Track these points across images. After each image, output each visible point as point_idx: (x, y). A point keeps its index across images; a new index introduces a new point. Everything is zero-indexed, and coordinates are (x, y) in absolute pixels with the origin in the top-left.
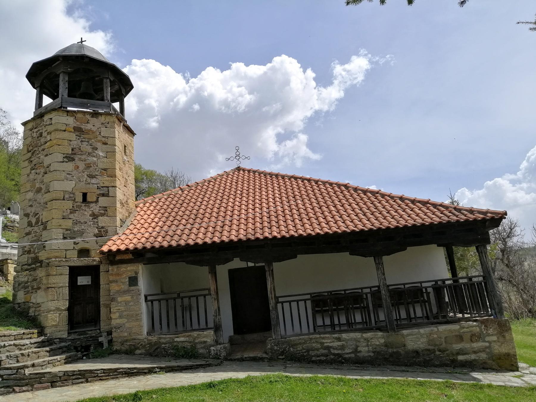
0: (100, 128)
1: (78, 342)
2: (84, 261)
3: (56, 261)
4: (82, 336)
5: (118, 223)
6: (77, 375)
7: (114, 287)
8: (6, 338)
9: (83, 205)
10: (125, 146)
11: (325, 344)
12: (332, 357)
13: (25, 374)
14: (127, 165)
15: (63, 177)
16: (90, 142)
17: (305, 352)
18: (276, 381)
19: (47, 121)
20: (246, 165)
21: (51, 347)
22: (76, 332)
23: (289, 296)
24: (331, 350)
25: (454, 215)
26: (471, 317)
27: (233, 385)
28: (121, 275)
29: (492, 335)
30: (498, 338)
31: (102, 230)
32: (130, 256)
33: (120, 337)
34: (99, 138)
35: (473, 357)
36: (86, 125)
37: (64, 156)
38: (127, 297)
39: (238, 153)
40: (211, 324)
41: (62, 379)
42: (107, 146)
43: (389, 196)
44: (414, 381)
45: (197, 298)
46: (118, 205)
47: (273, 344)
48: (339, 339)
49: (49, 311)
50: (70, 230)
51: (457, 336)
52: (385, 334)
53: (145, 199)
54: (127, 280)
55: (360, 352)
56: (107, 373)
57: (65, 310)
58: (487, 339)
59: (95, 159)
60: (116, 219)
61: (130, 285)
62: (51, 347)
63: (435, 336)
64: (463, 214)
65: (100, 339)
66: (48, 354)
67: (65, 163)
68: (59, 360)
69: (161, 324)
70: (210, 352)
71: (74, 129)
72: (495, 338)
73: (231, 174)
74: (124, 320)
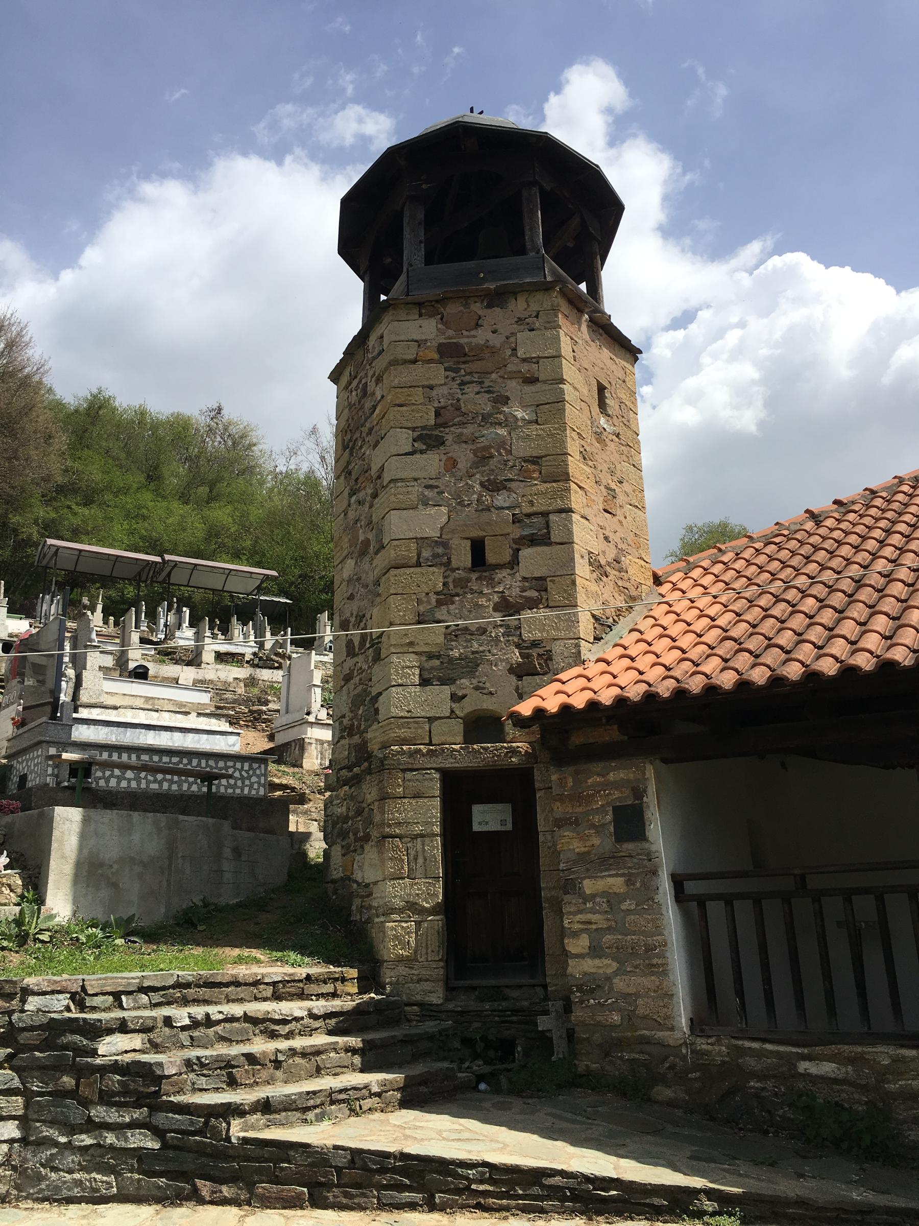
0: (513, 334)
1: (476, 1025)
2: (487, 752)
3: (403, 752)
5: (585, 627)
6: (394, 1170)
7: (571, 843)
8: (241, 992)
9: (474, 576)
10: (601, 389)
13: (228, 1139)
14: (612, 446)
15: (414, 497)
16: (487, 383)
19: (374, 347)
21: (371, 1036)
22: (474, 988)
28: (589, 799)
31: (534, 652)
32: (611, 734)
33: (599, 1024)
34: (511, 367)
36: (472, 333)
37: (416, 434)
38: (611, 880)
41: (345, 1180)
42: (539, 385)
46: (582, 569)
49: (389, 911)
50: (438, 657)
54: (609, 818)
57: (433, 911)
59: (502, 432)
62: (371, 1036)
66: (357, 1060)
67: (418, 456)
68: (375, 1089)
71: (439, 352)
74: (607, 966)
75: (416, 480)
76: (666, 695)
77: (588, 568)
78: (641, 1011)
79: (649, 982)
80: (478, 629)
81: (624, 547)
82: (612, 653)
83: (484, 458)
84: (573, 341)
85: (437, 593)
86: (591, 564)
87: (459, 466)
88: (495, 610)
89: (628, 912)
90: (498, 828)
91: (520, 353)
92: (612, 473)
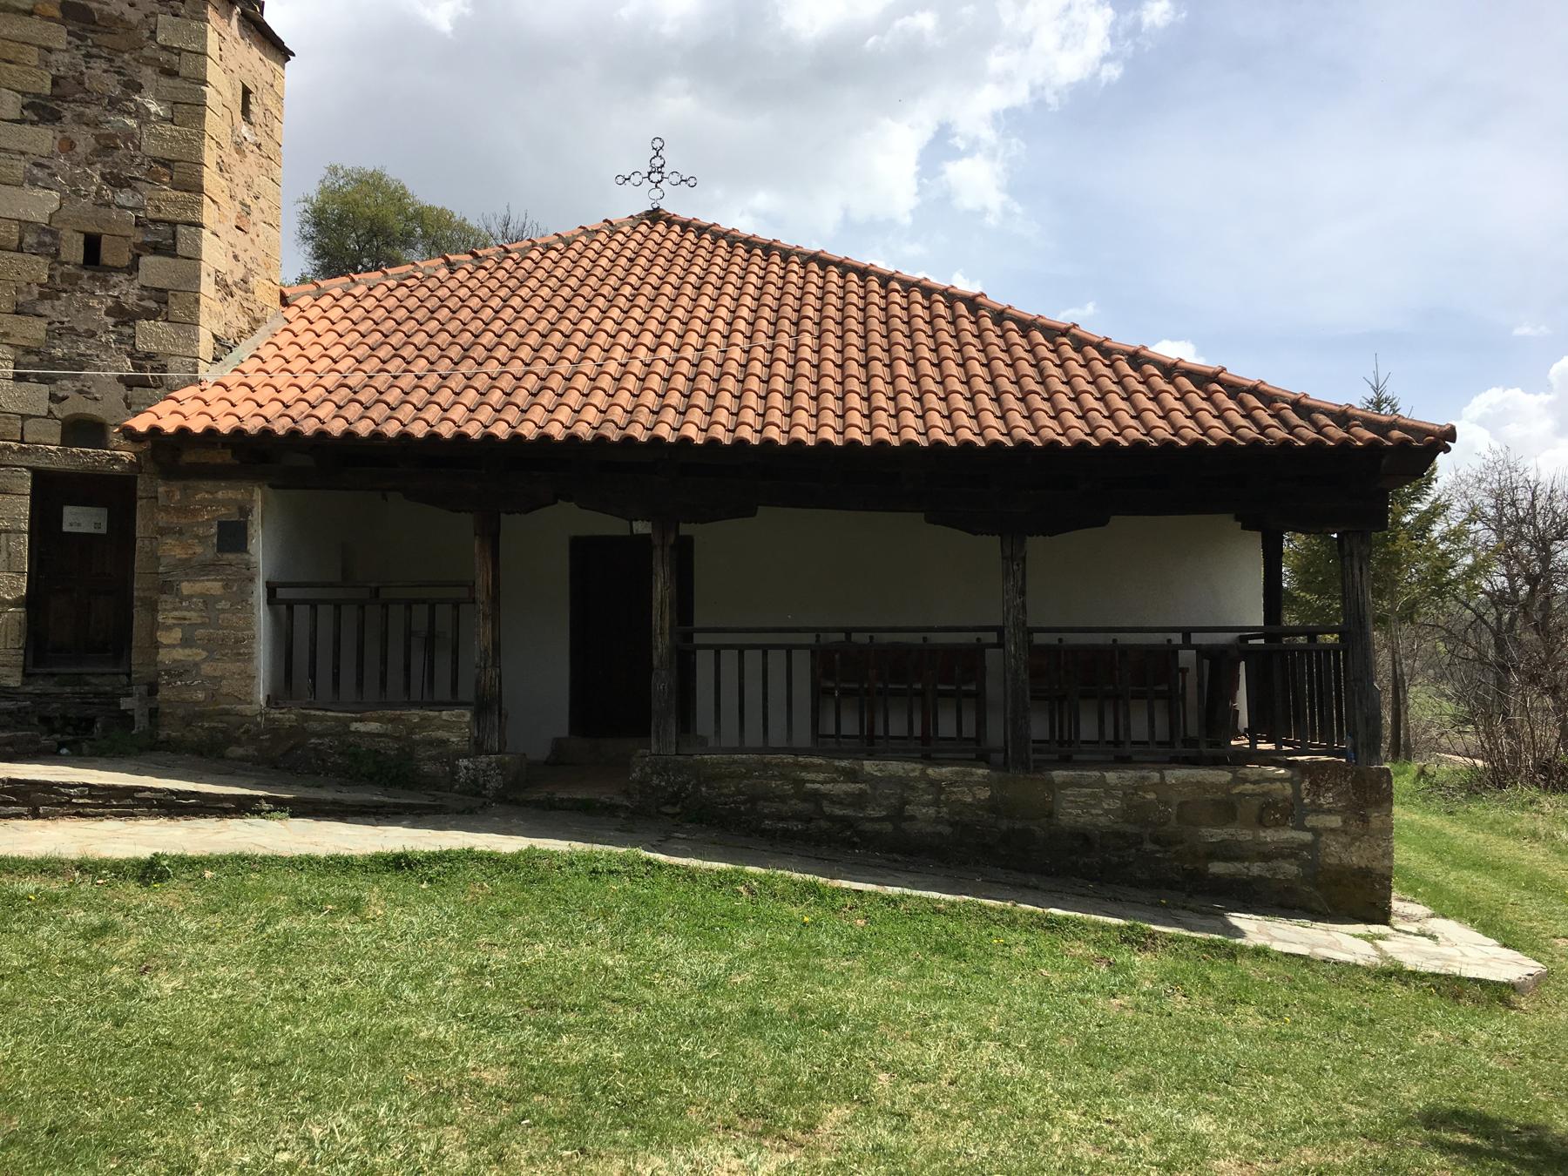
0: (154, 14)
2: (86, 457)
4: (68, 689)
5: (205, 347)
7: (172, 550)
10: (246, 92)
11: (809, 785)
12: (824, 824)
14: (251, 158)
15: (19, 173)
16: (118, 63)
17: (744, 803)
18: (611, 872)
20: (678, 205)
22: (53, 675)
23: (748, 631)
24: (825, 803)
25: (1285, 422)
26: (1278, 752)
27: (473, 870)
28: (195, 513)
29: (1329, 812)
30: (1344, 822)
32: (225, 457)
33: (184, 701)
34: (146, 52)
35: (1256, 869)
37: (26, 101)
38: (209, 584)
39: (657, 162)
40: (467, 692)
42: (178, 82)
43: (1098, 346)
44: (1031, 914)
45: (718, 653)
46: (207, 287)
47: (648, 770)
48: (852, 776)
50: (38, 353)
51: (1216, 803)
52: (995, 775)
53: (322, 284)
54: (214, 530)
55: (912, 818)
56: (100, 797)
57: (14, 604)
58: (1311, 821)
60: (197, 334)
61: (222, 547)
63: (1151, 796)
64: (1314, 423)
65: (125, 703)
67: (27, 126)
69: (313, 676)
70: (456, 773)
72: (1335, 821)
73: (626, 229)
75: (23, 153)
76: (281, 433)
77: (214, 287)
78: (224, 690)
79: (234, 667)
80: (86, 331)
81: (253, 266)
82: (232, 379)
83: (107, 147)
84: (222, 37)
85: (41, 285)
86: (217, 283)
87: (78, 149)
88: (107, 314)
89: (223, 611)
90: (92, 530)
91: (161, 38)
92: (249, 187)
